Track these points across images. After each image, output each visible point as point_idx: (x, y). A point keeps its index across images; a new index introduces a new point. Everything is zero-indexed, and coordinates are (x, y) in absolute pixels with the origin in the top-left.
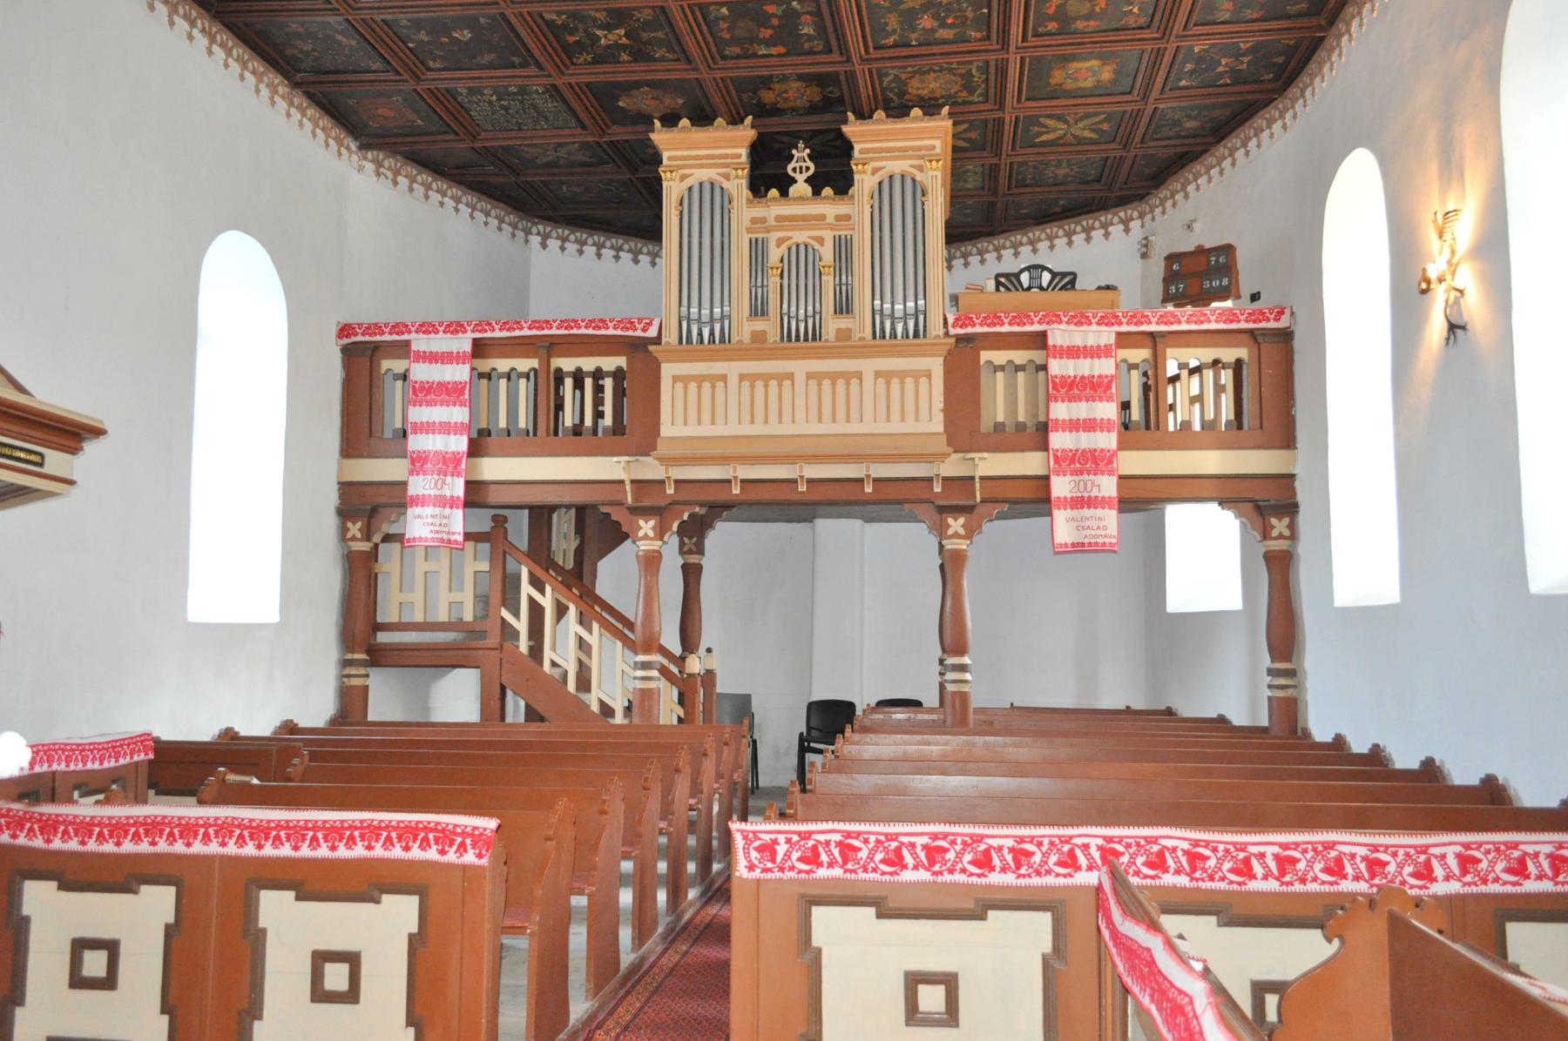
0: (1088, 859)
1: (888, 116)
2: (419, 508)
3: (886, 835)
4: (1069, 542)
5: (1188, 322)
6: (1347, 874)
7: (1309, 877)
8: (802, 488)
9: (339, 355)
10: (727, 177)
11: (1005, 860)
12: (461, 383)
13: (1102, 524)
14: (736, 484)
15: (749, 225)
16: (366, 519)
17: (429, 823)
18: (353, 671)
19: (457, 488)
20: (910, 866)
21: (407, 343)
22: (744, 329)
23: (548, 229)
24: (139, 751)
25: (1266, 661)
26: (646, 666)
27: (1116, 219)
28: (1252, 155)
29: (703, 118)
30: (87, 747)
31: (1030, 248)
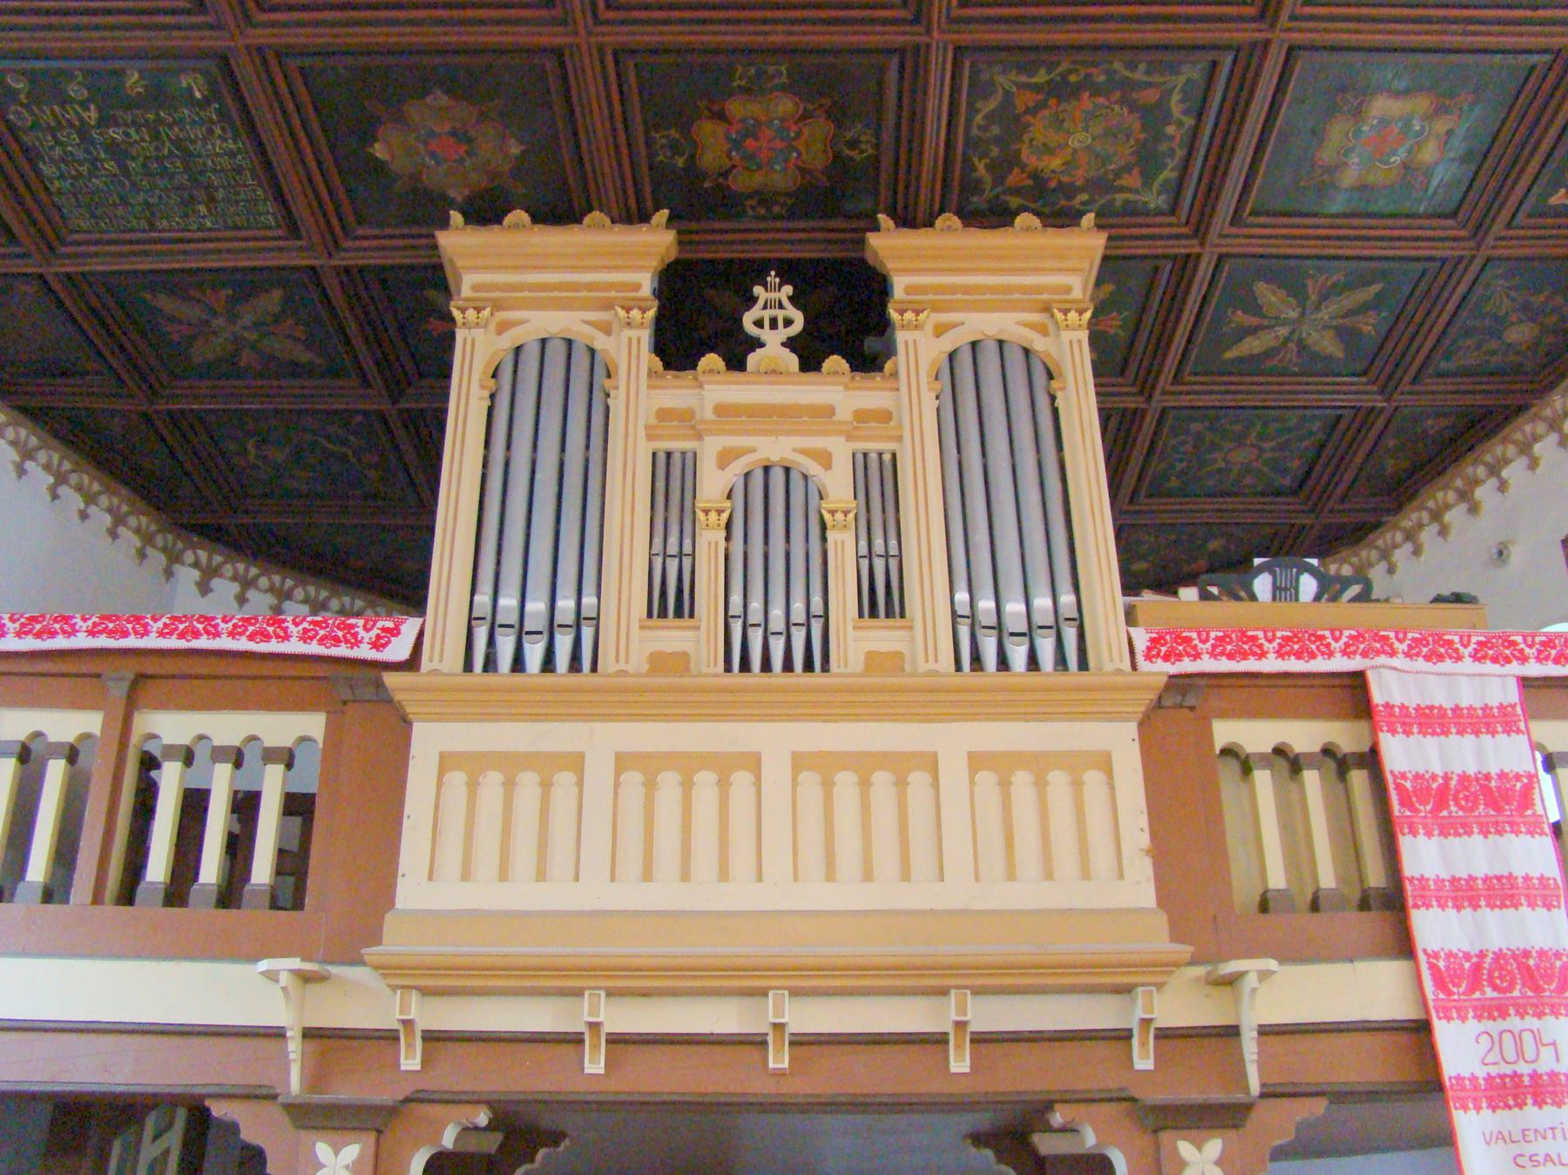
1: (966, 225)
14: (596, 1047)
15: (653, 421)
23: (218, 559)
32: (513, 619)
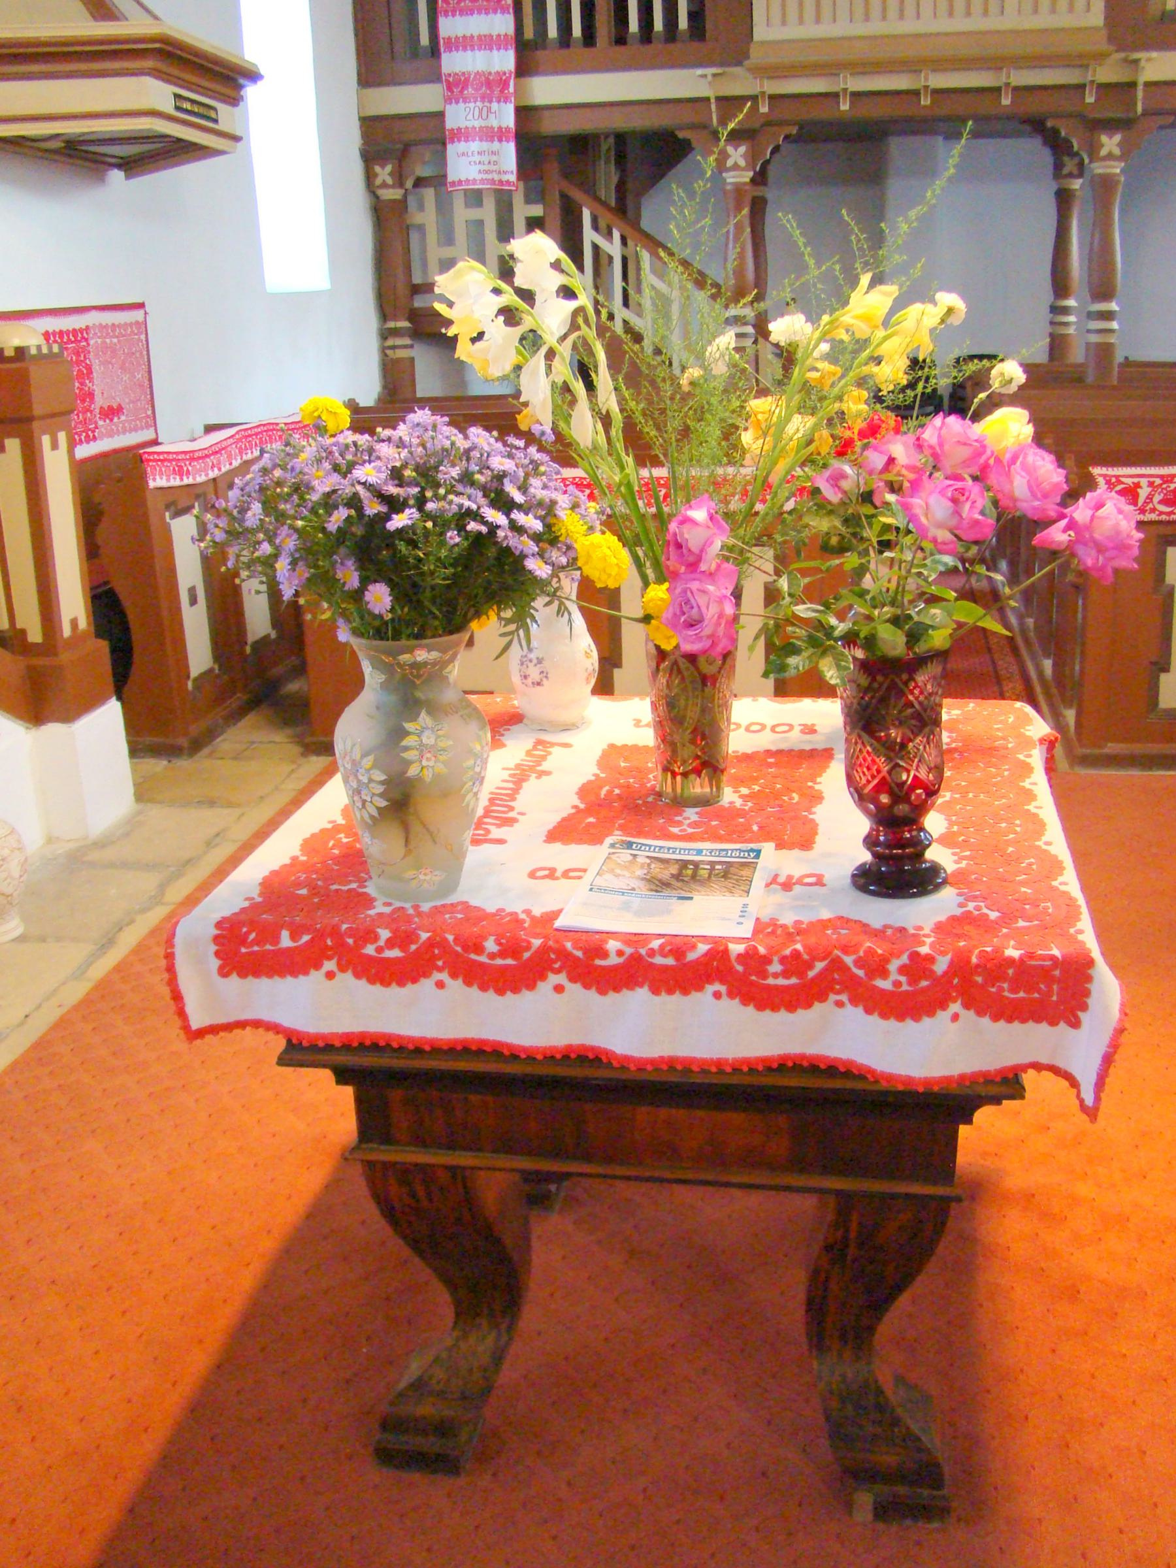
2: (463, 143)
19: (506, 117)
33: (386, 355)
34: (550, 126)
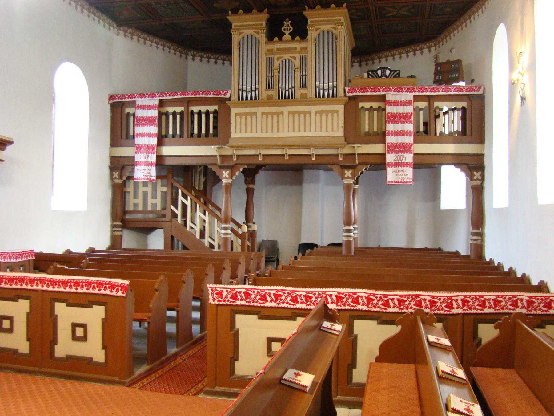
0: (332, 300)
3: (261, 290)
4: (393, 181)
5: (442, 91)
6: (268, 300)
7: (409, 307)
8: (287, 158)
9: (108, 107)
10: (258, 33)
11: (302, 299)
12: (154, 117)
13: (406, 173)
15: (266, 52)
16: (120, 171)
17: (107, 281)
18: (116, 229)
19: (153, 158)
20: (269, 301)
21: (135, 102)
22: (264, 94)
23: (195, 53)
24: (30, 256)
25: (471, 230)
26: (226, 229)
27: (425, 47)
28: (472, 22)
29: (248, 10)
30: (11, 254)
31: (392, 58)
32: (322, 87)
33: (113, 233)
34: (168, 162)
